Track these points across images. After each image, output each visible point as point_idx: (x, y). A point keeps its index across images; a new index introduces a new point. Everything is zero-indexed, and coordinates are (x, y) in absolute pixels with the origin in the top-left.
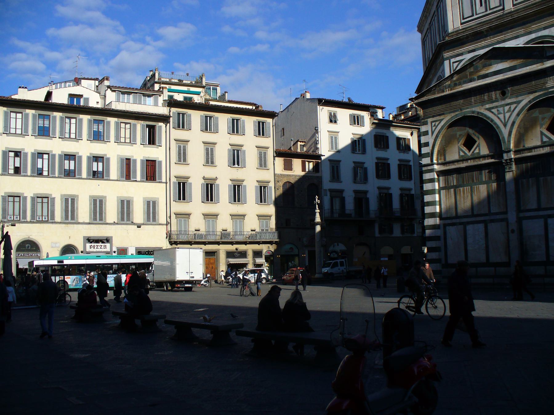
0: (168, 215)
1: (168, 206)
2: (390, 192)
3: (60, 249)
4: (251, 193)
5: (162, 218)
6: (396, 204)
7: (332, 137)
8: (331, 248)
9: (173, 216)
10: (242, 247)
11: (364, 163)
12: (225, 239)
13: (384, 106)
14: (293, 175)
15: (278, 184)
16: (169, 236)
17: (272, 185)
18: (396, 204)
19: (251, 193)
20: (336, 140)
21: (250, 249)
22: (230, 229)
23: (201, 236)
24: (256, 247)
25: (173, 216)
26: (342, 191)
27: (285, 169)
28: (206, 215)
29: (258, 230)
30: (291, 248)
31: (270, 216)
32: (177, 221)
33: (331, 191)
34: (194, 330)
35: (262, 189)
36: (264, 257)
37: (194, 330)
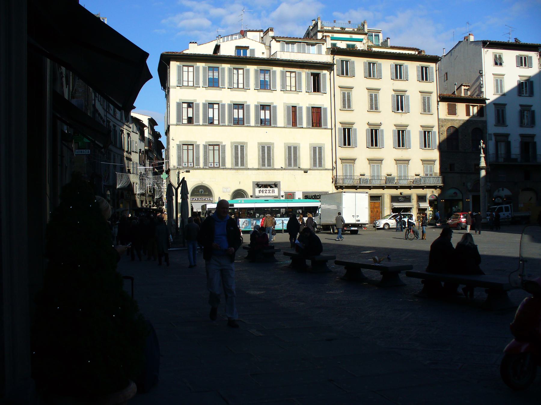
0: (334, 160)
3: (231, 193)
4: (415, 137)
5: (328, 163)
9: (339, 162)
14: (457, 120)
15: (442, 129)
16: (335, 180)
17: (436, 129)
19: (415, 137)
21: (414, 193)
23: (366, 181)
24: (420, 192)
25: (339, 162)
26: (507, 135)
27: (449, 113)
28: (370, 160)
30: (455, 193)
31: (434, 161)
32: (343, 166)
33: (496, 135)
34: (364, 271)
35: (426, 133)
36: (428, 201)
37: (364, 271)
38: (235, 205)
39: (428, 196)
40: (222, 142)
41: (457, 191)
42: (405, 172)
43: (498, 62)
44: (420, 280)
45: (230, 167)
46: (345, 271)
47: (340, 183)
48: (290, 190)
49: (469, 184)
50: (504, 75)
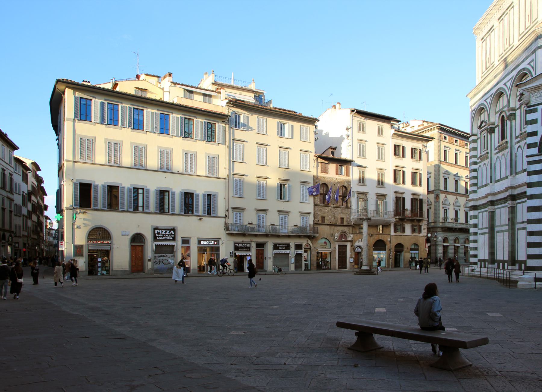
1: (227, 200)
2: (404, 196)
3: (129, 237)
5: (221, 209)
6: (408, 206)
7: (360, 145)
8: (356, 244)
9: (230, 210)
10: (246, 240)
11: (46, 195)
12: (274, 234)
13: (400, 120)
16: (227, 228)
18: (408, 206)
20: (363, 148)
21: (292, 243)
22: (277, 223)
23: (253, 229)
24: (299, 241)
25: (230, 210)
26: (365, 194)
28: (258, 210)
29: (299, 225)
30: (325, 243)
31: (309, 213)
33: (359, 193)
34: (376, 336)
37: (376, 336)
38: (78, 242)
39: (304, 246)
40: (122, 184)
41: (327, 242)
42: (285, 222)
43: (380, 132)
44: (354, 332)
45: (153, 212)
46: (355, 338)
47: (232, 228)
48: (186, 236)
49: (336, 235)
50: (385, 144)
